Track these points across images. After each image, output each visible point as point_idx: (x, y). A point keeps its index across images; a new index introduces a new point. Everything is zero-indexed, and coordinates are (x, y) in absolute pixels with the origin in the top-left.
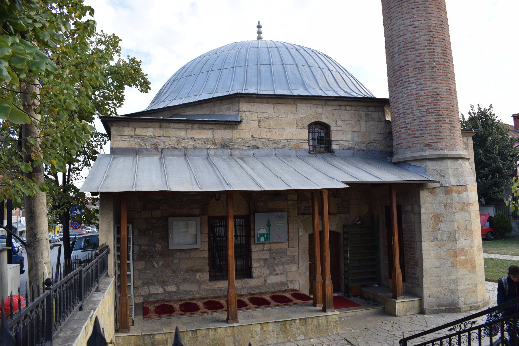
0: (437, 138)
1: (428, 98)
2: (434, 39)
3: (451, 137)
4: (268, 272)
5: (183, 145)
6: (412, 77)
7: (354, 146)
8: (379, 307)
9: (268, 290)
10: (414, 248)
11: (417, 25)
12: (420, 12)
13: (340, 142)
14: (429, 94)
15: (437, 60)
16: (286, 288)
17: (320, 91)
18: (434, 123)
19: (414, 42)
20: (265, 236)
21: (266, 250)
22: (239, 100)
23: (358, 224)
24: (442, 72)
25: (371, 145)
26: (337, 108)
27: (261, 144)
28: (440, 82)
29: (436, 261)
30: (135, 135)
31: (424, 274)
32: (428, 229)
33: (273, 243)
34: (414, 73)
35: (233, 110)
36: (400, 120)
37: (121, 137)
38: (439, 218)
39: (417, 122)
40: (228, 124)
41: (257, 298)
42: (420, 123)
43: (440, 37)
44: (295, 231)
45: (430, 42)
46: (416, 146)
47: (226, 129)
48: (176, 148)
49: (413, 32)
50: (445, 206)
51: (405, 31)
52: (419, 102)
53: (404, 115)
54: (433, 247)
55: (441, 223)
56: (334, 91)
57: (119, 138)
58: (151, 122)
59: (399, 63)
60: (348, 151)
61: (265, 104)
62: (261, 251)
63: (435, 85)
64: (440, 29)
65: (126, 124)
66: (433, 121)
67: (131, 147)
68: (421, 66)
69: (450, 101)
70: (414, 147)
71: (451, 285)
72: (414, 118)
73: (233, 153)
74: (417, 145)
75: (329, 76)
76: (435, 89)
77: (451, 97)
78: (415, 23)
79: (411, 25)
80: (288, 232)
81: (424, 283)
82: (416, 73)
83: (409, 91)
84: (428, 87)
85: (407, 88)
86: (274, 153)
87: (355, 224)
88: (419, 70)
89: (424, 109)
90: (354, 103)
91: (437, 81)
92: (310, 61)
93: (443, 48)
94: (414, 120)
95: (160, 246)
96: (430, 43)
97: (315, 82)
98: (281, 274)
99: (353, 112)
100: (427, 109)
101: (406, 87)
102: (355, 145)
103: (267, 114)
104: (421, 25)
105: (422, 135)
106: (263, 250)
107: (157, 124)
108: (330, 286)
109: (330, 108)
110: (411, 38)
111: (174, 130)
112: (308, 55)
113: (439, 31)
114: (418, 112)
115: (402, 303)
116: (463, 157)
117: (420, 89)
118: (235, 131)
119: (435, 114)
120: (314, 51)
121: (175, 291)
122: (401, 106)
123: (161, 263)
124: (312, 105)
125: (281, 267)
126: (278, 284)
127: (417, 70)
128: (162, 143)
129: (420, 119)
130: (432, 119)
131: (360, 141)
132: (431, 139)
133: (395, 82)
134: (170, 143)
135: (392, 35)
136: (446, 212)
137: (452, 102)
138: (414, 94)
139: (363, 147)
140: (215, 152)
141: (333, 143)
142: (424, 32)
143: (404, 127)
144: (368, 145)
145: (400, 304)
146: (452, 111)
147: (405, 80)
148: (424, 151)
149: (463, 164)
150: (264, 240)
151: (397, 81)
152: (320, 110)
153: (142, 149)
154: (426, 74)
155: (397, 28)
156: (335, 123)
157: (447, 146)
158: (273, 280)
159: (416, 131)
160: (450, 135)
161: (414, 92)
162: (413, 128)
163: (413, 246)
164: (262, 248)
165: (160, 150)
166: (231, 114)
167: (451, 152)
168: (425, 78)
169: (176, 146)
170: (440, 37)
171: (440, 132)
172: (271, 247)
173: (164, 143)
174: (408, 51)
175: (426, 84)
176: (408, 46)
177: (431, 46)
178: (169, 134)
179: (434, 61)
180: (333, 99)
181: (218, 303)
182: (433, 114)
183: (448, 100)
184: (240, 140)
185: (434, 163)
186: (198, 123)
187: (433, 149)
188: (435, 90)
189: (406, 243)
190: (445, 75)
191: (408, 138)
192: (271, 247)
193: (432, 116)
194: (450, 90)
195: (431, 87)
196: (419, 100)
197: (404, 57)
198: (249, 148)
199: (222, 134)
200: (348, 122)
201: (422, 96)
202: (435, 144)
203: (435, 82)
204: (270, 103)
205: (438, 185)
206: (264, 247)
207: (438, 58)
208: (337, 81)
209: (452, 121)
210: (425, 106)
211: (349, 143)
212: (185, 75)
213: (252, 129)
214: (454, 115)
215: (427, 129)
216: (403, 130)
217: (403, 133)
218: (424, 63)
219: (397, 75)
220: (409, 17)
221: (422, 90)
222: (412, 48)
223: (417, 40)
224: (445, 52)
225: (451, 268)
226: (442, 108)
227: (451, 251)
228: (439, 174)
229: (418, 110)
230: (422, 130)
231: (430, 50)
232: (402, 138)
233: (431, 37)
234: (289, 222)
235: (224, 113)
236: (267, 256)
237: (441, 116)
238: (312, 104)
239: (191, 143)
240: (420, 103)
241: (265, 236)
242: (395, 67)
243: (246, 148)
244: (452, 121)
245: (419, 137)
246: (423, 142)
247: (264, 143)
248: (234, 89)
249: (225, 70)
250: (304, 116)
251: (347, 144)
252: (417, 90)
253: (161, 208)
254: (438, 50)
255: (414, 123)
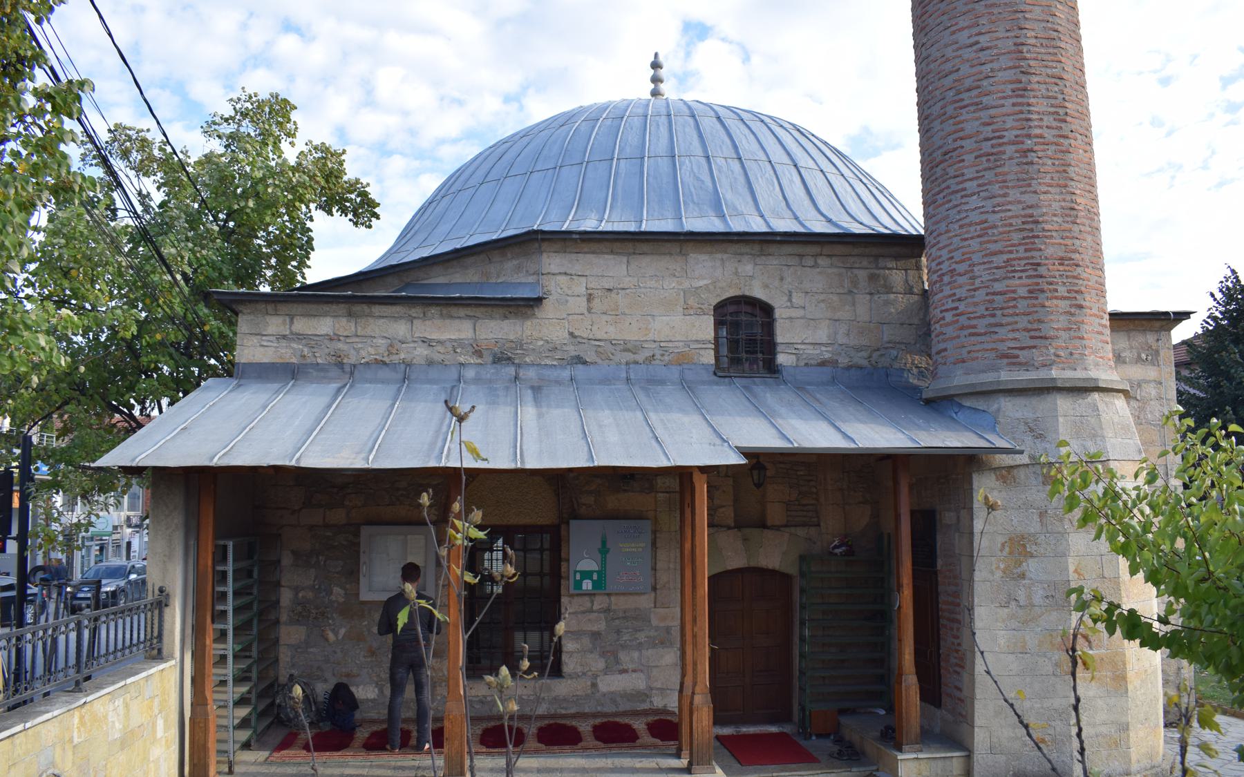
0: (1032, 337)
1: (1009, 232)
2: (1029, 76)
3: (1072, 333)
4: (601, 664)
5: (402, 356)
6: (971, 180)
7: (835, 358)
8: (861, 769)
9: (599, 709)
10: (959, 622)
11: (985, 45)
12: (996, 11)
13: (799, 346)
14: (1013, 221)
15: (1038, 131)
16: (646, 706)
17: (759, 219)
18: (1025, 298)
19: (978, 87)
20: (595, 577)
21: (599, 611)
22: (540, 247)
23: (836, 554)
24: (1049, 162)
25: (882, 355)
26: (795, 261)
27: (593, 353)
28: (1045, 189)
29: (1012, 657)
30: (292, 333)
31: (978, 691)
32: (992, 573)
33: (616, 594)
34: (976, 168)
35: (527, 271)
36: (942, 291)
37: (259, 337)
38: (1024, 546)
39: (981, 295)
40: (509, 306)
41: (617, 724)
42: (988, 298)
43: (1049, 71)
44: (672, 566)
45: (1020, 86)
46: (977, 358)
47: (506, 317)
48: (384, 363)
49: (975, 62)
50: (1042, 514)
51: (957, 60)
52: (989, 242)
53: (952, 277)
54: (1004, 621)
55: (1030, 561)
56: (796, 218)
57: (255, 340)
58: (327, 303)
59: (941, 143)
60: (820, 369)
61: (606, 256)
62: (584, 612)
63: (1029, 199)
64: (1051, 50)
65: (270, 308)
66: (1022, 292)
67: (281, 361)
68: (994, 150)
69: (1073, 238)
70: (973, 359)
71: (1053, 723)
72: (973, 284)
73: (521, 375)
74: (980, 354)
75: (791, 181)
76: (1031, 207)
77: (1076, 228)
78: (982, 39)
79: (971, 46)
80: (654, 569)
81: (976, 714)
82: (980, 168)
83: (964, 215)
84: (1010, 203)
85: (958, 209)
86: (624, 375)
87: (831, 553)
88: (988, 160)
89: (999, 260)
90: (839, 249)
91: (1035, 186)
92: (748, 146)
93: (1058, 101)
94: (975, 290)
95: (342, 592)
96: (1019, 89)
97: (749, 199)
98: (634, 671)
99: (835, 270)
100: (1008, 260)
101: (956, 206)
102: (840, 354)
103: (610, 279)
104: (995, 43)
105: (992, 330)
106: (591, 611)
107: (341, 308)
108: (706, 709)
109: (774, 261)
110: (973, 78)
111: (383, 320)
112: (747, 131)
113: (1045, 57)
114: (985, 270)
115: (916, 763)
116: (1102, 385)
117: (991, 209)
118: (528, 323)
119: (1027, 274)
120: (767, 120)
121: (374, 699)
122: (944, 252)
123: (342, 631)
124: (725, 256)
125: (636, 654)
126: (627, 696)
127: (984, 159)
128: (352, 352)
129: (988, 287)
130: (1020, 285)
131: (852, 344)
132: (1015, 339)
133: (933, 192)
134: (372, 351)
135: (928, 73)
136: (1044, 530)
137: (1077, 242)
138: (976, 224)
139: (860, 359)
140: (477, 373)
141: (779, 349)
142: (1005, 62)
143: (952, 309)
144: (876, 355)
145: (912, 765)
146: (1077, 265)
147: (954, 188)
148: (995, 369)
149: (1101, 406)
150: (590, 587)
151: (937, 189)
152: (748, 268)
153: (306, 365)
154: (1006, 169)
155: (939, 54)
156: (786, 298)
157: (1058, 356)
158: (612, 684)
159: (979, 317)
160: (1070, 329)
161: (975, 217)
162: (970, 309)
163: (958, 617)
164: (589, 605)
165: (347, 369)
166: (524, 280)
167: (1069, 374)
168: (1005, 181)
169: (387, 360)
170: (1049, 71)
171: (1039, 321)
172: (610, 604)
173: (357, 350)
174: (964, 111)
175: (1005, 195)
176: (962, 100)
177: (1022, 96)
178: (369, 331)
179: (1029, 136)
180: (778, 238)
181: (628, 727)
182: (1024, 275)
183: (1067, 237)
184: (541, 343)
185: (1020, 401)
186: (437, 305)
187: (1020, 364)
188: (1030, 211)
189: (944, 607)
190: (1057, 172)
191: (958, 337)
192: (610, 604)
193: (1020, 278)
194: (1073, 209)
195: (1019, 202)
196: (986, 239)
197: (954, 128)
198: (563, 362)
199: (497, 330)
200: (822, 297)
201: (994, 227)
202: (1025, 352)
203: (1029, 189)
204: (617, 254)
205: (1024, 459)
206: (592, 602)
207: (1041, 127)
208: (814, 192)
209: (1076, 292)
210: (1001, 252)
211: (824, 348)
212: (453, 189)
213: (570, 317)
214: (1084, 275)
215: (1005, 312)
216: (949, 317)
217: (948, 325)
218: (1001, 141)
219: (938, 175)
220: (966, 24)
221: (994, 212)
222: (972, 104)
223: (985, 83)
224: (1061, 111)
225: (1053, 678)
226: (1046, 258)
227: (1054, 634)
228: (1032, 430)
229: (984, 263)
230: (993, 316)
231: (1017, 108)
232: (947, 336)
233: (1022, 72)
234: (658, 545)
235: (509, 279)
236: (601, 626)
237: (1044, 280)
238: (726, 252)
239: (421, 352)
240: (989, 246)
241: (595, 577)
242: (935, 155)
243: (555, 363)
244: (1076, 292)
245: (985, 334)
246: (993, 346)
247: (599, 349)
248: (547, 220)
249: (535, 175)
250: (705, 282)
251: (818, 352)
252: (982, 213)
253: (347, 503)
254: (1040, 106)
255: (973, 297)
